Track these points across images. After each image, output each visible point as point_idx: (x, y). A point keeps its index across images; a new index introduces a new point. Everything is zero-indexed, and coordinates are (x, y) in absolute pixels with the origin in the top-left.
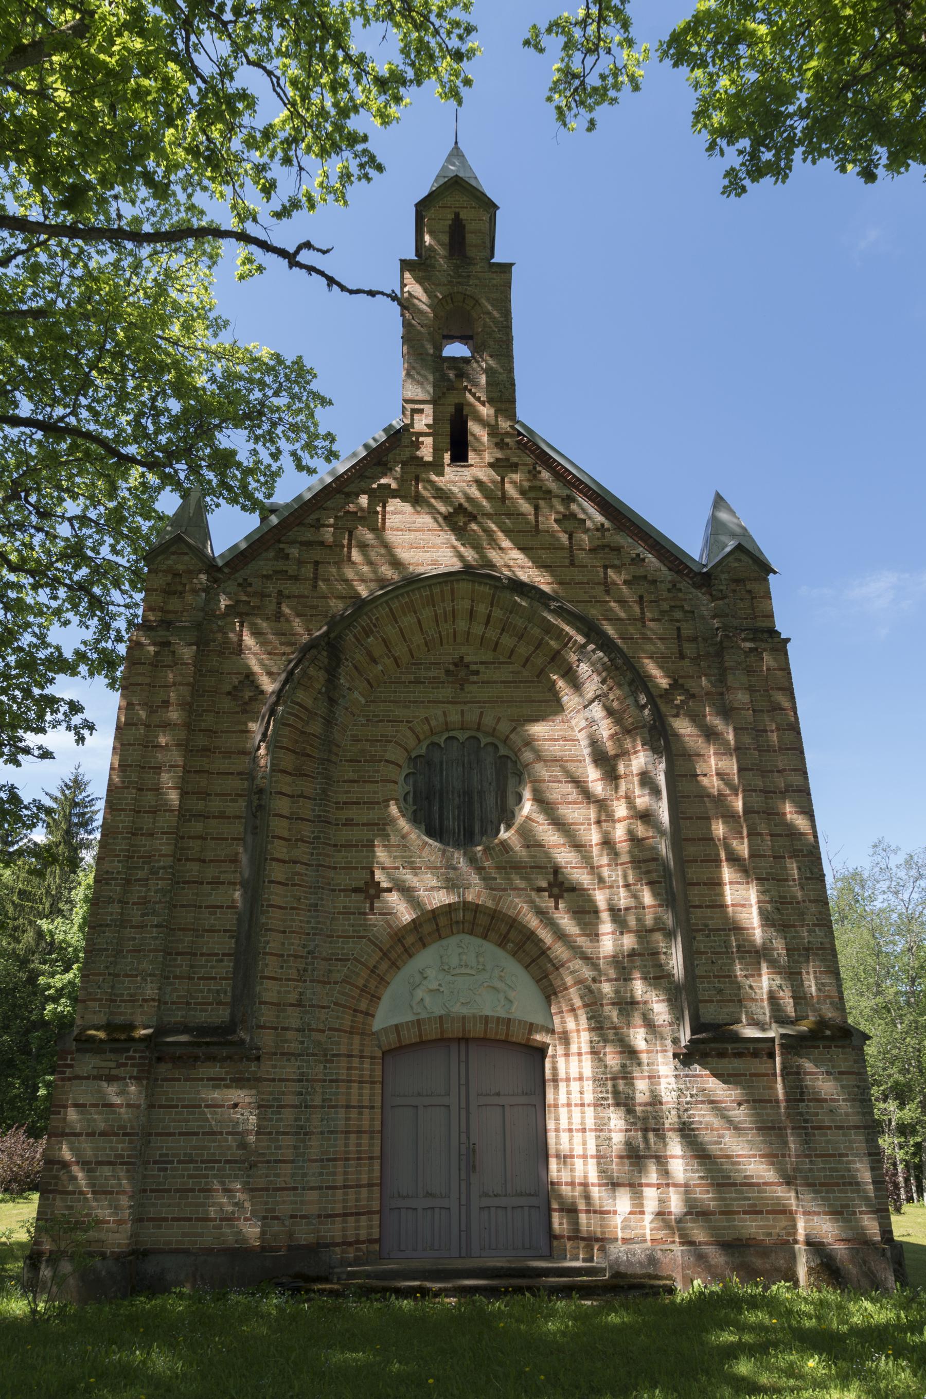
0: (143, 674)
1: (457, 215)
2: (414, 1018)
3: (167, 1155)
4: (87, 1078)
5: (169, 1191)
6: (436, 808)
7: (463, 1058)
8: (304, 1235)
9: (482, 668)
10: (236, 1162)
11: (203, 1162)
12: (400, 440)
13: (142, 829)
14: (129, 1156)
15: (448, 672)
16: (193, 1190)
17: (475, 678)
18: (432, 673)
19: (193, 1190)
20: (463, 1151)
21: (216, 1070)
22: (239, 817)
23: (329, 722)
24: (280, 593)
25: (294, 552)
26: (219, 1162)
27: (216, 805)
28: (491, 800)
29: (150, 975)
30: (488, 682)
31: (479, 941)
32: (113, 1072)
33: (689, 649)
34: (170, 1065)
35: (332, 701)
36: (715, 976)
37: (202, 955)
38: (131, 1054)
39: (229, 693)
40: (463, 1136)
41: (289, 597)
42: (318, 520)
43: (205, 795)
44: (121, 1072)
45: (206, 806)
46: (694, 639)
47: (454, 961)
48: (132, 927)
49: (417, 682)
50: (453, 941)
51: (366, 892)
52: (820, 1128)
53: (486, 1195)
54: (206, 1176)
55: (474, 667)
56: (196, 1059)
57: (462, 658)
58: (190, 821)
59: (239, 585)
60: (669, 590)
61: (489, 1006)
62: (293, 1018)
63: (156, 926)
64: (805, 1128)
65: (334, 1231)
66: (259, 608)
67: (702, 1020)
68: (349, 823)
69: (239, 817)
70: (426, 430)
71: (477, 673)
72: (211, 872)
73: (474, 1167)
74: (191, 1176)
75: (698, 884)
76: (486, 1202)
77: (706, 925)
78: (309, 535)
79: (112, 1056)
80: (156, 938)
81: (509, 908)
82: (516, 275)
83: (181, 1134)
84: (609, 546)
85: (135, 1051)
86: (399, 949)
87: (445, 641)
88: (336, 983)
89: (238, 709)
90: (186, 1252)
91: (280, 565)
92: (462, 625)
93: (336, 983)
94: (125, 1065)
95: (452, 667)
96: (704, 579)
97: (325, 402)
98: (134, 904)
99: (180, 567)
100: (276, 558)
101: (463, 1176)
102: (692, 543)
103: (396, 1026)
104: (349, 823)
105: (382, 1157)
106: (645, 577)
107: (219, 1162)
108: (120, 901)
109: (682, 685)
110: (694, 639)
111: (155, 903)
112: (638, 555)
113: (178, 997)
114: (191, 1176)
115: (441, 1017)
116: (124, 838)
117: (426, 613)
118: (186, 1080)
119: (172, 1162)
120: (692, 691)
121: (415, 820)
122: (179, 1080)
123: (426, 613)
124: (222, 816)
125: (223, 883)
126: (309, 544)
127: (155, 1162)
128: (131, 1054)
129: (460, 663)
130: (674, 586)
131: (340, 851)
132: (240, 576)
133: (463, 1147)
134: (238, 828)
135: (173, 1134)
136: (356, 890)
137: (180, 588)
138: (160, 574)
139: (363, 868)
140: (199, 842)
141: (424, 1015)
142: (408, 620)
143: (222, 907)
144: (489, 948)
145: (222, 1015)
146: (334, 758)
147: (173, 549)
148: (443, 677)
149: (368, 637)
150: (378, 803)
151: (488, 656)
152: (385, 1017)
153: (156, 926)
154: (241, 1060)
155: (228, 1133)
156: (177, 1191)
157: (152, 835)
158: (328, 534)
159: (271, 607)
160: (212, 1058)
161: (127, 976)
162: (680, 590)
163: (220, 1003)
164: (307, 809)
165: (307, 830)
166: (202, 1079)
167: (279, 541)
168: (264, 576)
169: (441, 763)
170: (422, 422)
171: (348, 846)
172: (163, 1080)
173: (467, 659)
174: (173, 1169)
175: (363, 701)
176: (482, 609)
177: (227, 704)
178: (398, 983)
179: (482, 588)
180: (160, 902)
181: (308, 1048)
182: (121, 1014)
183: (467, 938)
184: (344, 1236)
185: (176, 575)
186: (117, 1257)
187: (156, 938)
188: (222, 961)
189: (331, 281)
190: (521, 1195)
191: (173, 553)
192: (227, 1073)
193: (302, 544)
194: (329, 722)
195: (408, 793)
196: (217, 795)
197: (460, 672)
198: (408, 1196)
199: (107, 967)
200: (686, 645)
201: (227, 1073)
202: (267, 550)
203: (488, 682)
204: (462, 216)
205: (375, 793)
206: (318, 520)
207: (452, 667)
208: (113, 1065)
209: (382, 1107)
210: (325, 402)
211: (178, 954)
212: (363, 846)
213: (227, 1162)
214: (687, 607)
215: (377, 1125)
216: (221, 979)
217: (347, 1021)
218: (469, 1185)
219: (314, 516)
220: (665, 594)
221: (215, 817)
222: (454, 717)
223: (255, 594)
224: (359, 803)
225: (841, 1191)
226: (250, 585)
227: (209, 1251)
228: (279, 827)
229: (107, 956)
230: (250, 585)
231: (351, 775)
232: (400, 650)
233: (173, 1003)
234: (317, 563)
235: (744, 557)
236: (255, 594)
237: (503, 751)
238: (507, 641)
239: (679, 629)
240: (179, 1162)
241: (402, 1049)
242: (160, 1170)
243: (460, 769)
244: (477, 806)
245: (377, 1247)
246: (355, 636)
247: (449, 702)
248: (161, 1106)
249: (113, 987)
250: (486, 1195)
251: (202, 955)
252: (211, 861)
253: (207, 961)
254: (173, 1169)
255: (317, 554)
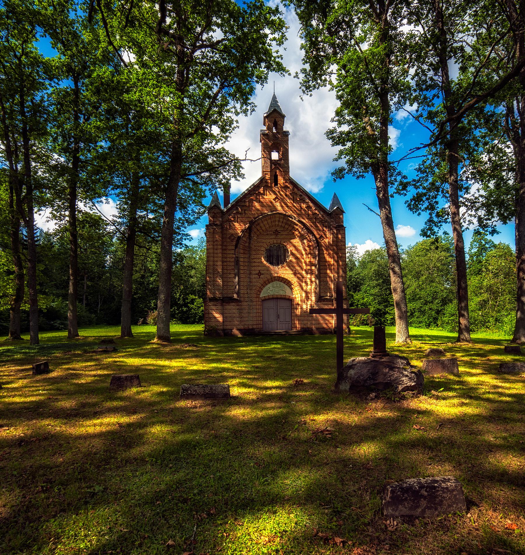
8: (251, 327)
23: (249, 243)
27: (228, 259)
28: (283, 257)
35: (250, 239)
43: (226, 258)
62: (246, 296)
65: (255, 327)
68: (255, 262)
70: (215, 28)
72: (229, 271)
78: (243, 204)
92: (277, 223)
97: (242, 168)
104: (255, 262)
117: (269, 221)
121: (267, 261)
123: (269, 221)
129: (276, 231)
134: (233, 264)
142: (265, 222)
144: (282, 283)
151: (282, 229)
152: (262, 295)
158: (247, 204)
164: (246, 260)
165: (247, 264)
170: (268, 177)
176: (281, 220)
177: (228, 240)
178: (264, 289)
189: (251, 160)
194: (249, 243)
197: (276, 233)
210: (242, 168)
217: (255, 296)
222: (275, 242)
228: (241, 263)
232: (264, 228)
238: (287, 226)
241: (265, 300)
255: (245, 208)
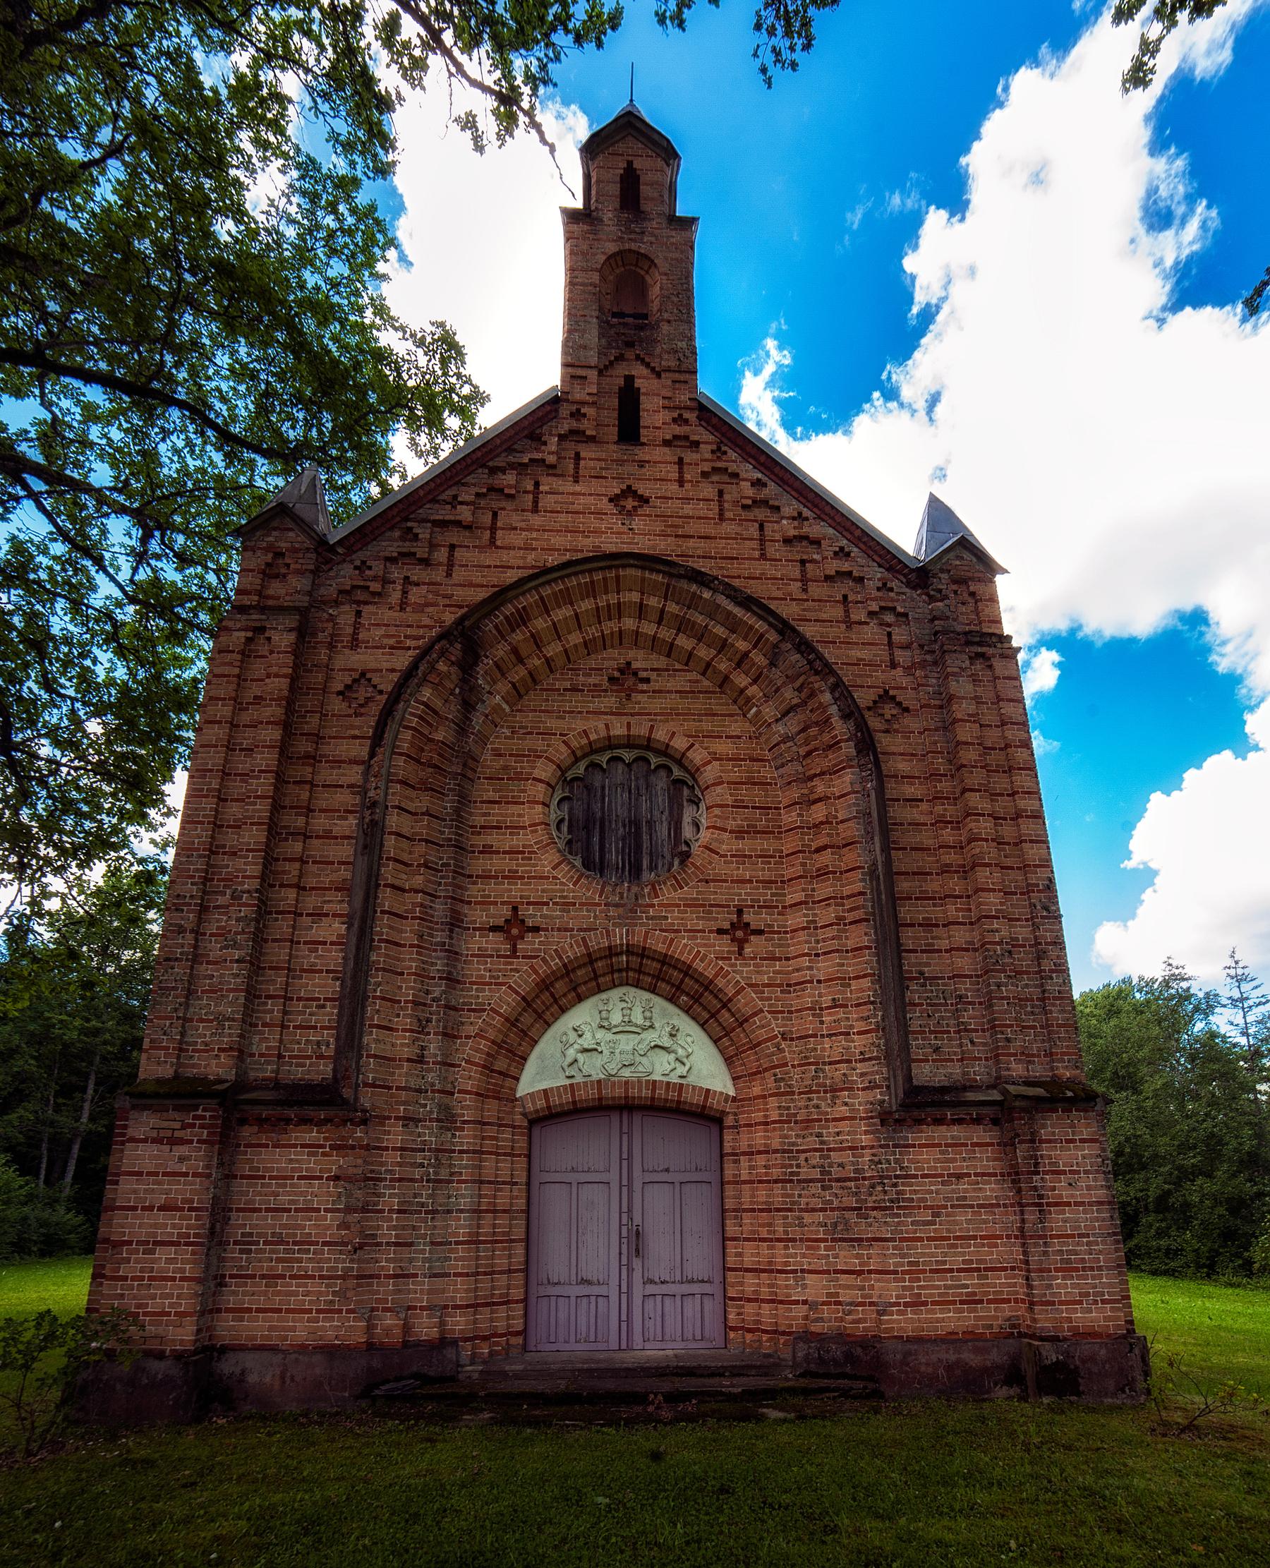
0: (230, 664)
1: (630, 163)
2: (568, 1082)
3: (251, 1234)
4: (145, 1141)
5: (253, 1277)
6: (596, 839)
7: (625, 1129)
9: (653, 675)
10: (336, 1244)
11: (295, 1243)
12: (557, 411)
13: (224, 846)
14: (196, 1236)
15: (612, 680)
16: (283, 1277)
17: (645, 687)
18: (591, 680)
19: (283, 1277)
20: (624, 1234)
21: (313, 1135)
22: (349, 837)
23: (462, 729)
24: (407, 578)
25: (423, 532)
26: (317, 1243)
29: (228, 1019)
30: (660, 692)
31: (647, 995)
32: (177, 1134)
33: (902, 656)
34: (256, 1128)
36: (931, 1032)
37: (299, 999)
38: (200, 1112)
39: (339, 693)
40: (625, 1216)
41: (417, 584)
42: (455, 497)
44: (185, 1135)
45: (307, 823)
46: (907, 647)
47: (616, 1018)
48: (208, 963)
49: (574, 689)
50: (615, 994)
51: (508, 932)
52: (1057, 1204)
53: (652, 1282)
54: (300, 1260)
55: (643, 674)
56: (288, 1121)
57: (629, 664)
58: (286, 840)
59: (356, 568)
60: (879, 589)
61: (661, 1068)
63: (237, 961)
64: (1040, 1205)
66: (379, 594)
67: (915, 1083)
69: (349, 837)
71: (647, 680)
73: (637, 1251)
74: (279, 1260)
75: (912, 925)
76: (651, 1289)
77: (922, 973)
78: (444, 513)
79: (176, 1115)
80: (237, 975)
81: (682, 953)
82: (701, 235)
83: (267, 1210)
84: (806, 538)
85: (204, 1110)
86: (546, 996)
87: (608, 643)
88: (468, 1037)
89: (351, 711)
90: (273, 1349)
91: (407, 547)
93: (468, 1037)
94: (193, 1126)
95: (616, 674)
96: (919, 576)
98: (212, 935)
99: (283, 545)
100: (402, 539)
101: (624, 1261)
102: (904, 532)
103: (545, 1091)
105: (527, 1240)
106: (850, 573)
107: (317, 1243)
108: (192, 931)
109: (893, 698)
110: (907, 647)
111: (237, 933)
112: (842, 549)
113: (268, 1048)
114: (279, 1260)
115: (599, 1082)
116: (200, 856)
118: (275, 1146)
119: (258, 1243)
120: (905, 704)
122: (267, 1146)
124: (327, 836)
125: (327, 915)
126: (443, 524)
127: (236, 1243)
128: (200, 1112)
129: (627, 669)
130: (885, 584)
131: (475, 883)
132: (358, 558)
133: (624, 1229)
135: (259, 1210)
136: (494, 929)
137: (283, 571)
138: (259, 553)
139: (503, 903)
140: (297, 865)
141: (579, 1079)
143: (325, 943)
145: (325, 1070)
146: (470, 774)
147: (275, 524)
148: (606, 684)
149: (513, 631)
150: (524, 828)
153: (237, 961)
154: (344, 1122)
155: (326, 1210)
156: (263, 1277)
157: (235, 854)
159: (395, 597)
160: (305, 1121)
161: (202, 1021)
162: (891, 590)
163: (321, 1057)
166: (295, 1146)
167: (407, 519)
168: (387, 559)
169: (603, 788)
171: (486, 877)
172: (246, 1146)
173: (635, 665)
174: (259, 1251)
175: (507, 709)
179: (654, 576)
180: (243, 932)
181: (431, 1112)
182: (193, 1066)
183: (632, 991)
184: (509, 1326)
185: (279, 554)
186: (178, 1356)
187: (237, 975)
188: (323, 1006)
190: (692, 1281)
191: (275, 529)
192: (326, 1139)
193: (436, 523)
194: (462, 729)
195: (562, 821)
196: (322, 811)
198: (558, 1283)
199: (176, 1010)
200: (898, 652)
201: (326, 1139)
202: (392, 528)
203: (660, 692)
204: (637, 164)
205: (520, 815)
206: (455, 497)
207: (616, 674)
208: (177, 1125)
209: (528, 1184)
211: (269, 997)
212: (504, 877)
213: (325, 1244)
214: (900, 609)
215: (521, 1203)
216: (323, 1028)
218: (630, 1270)
219: (450, 492)
220: (875, 593)
221: (318, 837)
223: (375, 579)
224: (500, 828)
225: (1079, 1277)
226: (370, 568)
227: (302, 1349)
229: (176, 997)
230: (370, 568)
231: (491, 795)
233: (261, 1055)
234: (452, 547)
235: (967, 555)
236: (375, 579)
237: (677, 772)
238: (684, 642)
239: (889, 634)
240: (265, 1243)
242: (241, 1251)
243: (626, 795)
244: (645, 837)
245: (520, 1340)
246: (496, 627)
247: (612, 714)
248: (243, 1177)
249: (183, 1034)
250: (652, 1282)
251: (299, 999)
252: (313, 889)
253: (305, 1007)
254: (259, 1251)
255: (453, 536)
